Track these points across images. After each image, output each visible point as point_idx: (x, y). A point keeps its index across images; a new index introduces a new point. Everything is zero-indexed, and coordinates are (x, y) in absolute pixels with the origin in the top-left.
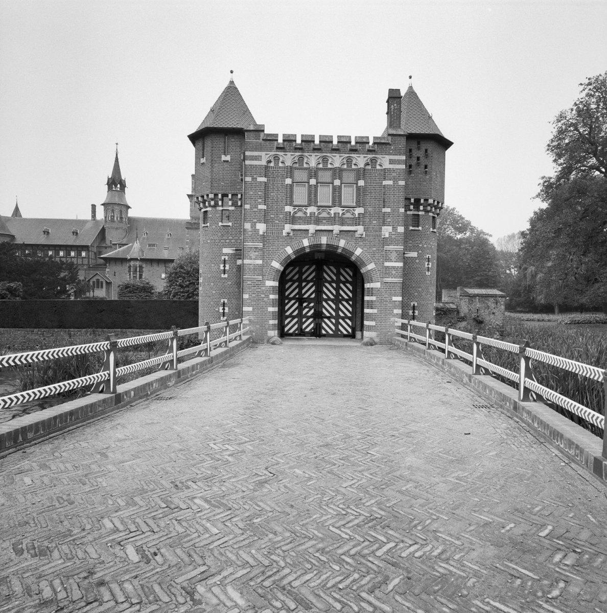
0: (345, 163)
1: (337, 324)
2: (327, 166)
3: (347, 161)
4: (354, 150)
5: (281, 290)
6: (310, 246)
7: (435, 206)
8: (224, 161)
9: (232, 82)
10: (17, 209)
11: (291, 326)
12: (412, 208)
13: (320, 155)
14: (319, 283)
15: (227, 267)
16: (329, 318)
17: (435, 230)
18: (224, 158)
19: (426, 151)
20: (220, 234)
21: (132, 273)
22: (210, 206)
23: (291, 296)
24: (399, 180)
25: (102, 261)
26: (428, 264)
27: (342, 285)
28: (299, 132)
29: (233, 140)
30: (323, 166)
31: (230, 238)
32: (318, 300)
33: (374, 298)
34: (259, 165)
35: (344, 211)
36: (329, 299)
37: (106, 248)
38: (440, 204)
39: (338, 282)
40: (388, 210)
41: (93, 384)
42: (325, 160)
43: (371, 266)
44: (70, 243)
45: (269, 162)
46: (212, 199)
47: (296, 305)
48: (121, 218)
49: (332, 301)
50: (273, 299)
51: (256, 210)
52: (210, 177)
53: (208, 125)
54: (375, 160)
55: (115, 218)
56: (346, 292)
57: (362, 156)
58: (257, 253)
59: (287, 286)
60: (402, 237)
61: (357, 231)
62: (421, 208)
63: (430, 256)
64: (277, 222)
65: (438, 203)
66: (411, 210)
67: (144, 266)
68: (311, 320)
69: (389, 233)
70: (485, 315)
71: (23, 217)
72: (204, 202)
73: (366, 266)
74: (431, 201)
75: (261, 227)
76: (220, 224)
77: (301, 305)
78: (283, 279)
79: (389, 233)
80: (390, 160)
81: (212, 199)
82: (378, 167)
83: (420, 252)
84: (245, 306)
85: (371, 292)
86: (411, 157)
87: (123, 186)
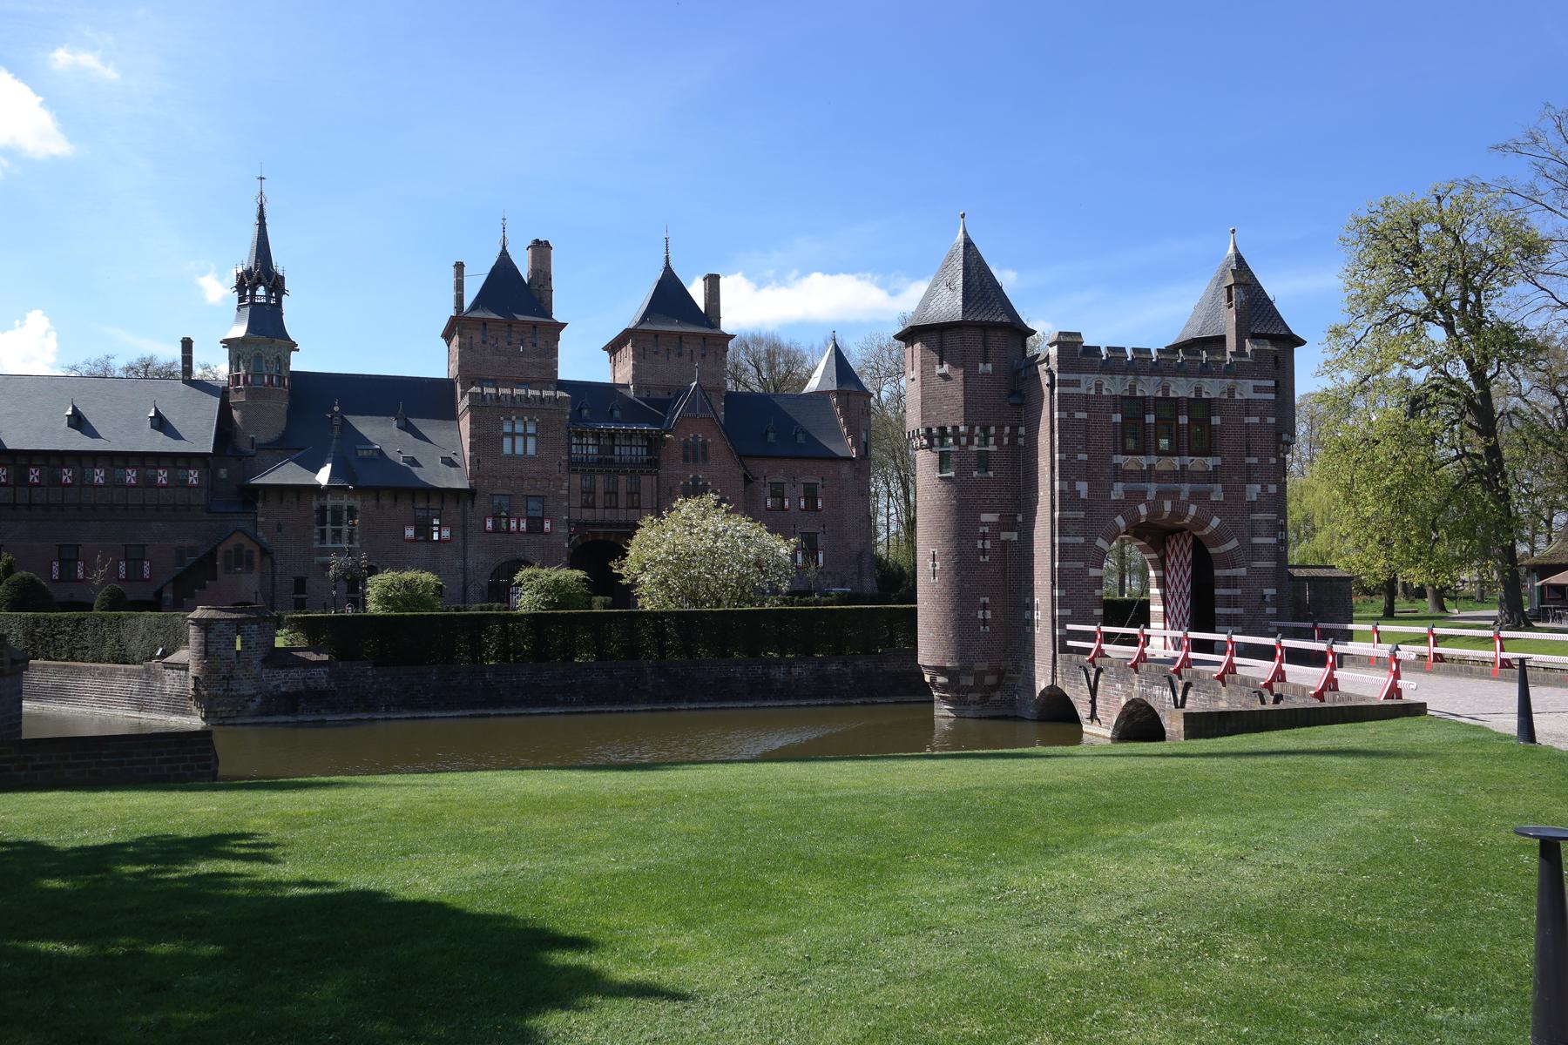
31: (992, 496)
51: (1074, 461)
58: (1077, 527)
62: (992, 440)
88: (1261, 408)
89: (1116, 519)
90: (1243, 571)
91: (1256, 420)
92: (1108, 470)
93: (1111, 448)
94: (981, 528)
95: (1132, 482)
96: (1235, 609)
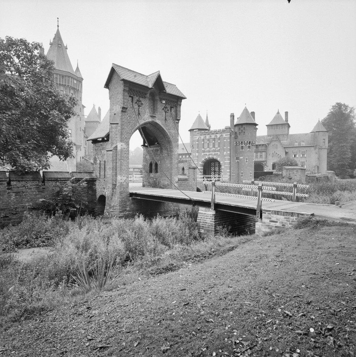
4: (217, 133)
9: (246, 107)
53: (237, 123)
70: (292, 176)
74: (246, 142)
75: (197, 154)
77: (215, 173)
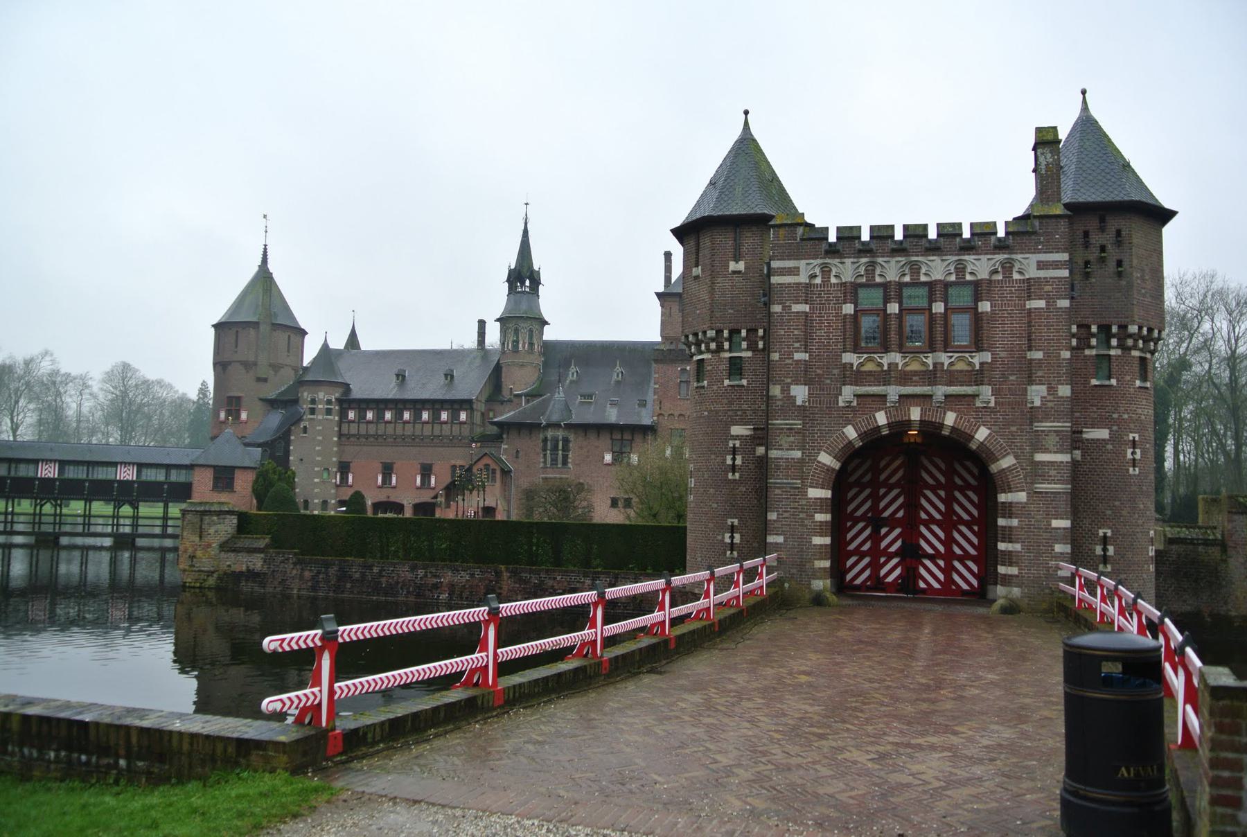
0: (952, 271)
1: (948, 570)
2: (919, 279)
3: (956, 268)
5: (837, 505)
6: (889, 425)
7: (1143, 338)
8: (734, 272)
10: (353, 334)
11: (858, 572)
12: (1095, 344)
13: (903, 259)
14: (912, 490)
15: (739, 461)
16: (932, 558)
17: (1148, 384)
18: (733, 266)
19: (1119, 233)
20: (725, 401)
21: (548, 452)
22: (708, 350)
23: (859, 513)
24: (1057, 299)
25: (495, 429)
26: (1133, 453)
27: (957, 494)
28: (865, 221)
29: (749, 234)
30: (911, 279)
31: (745, 407)
32: (910, 527)
33: (1015, 522)
34: (794, 284)
35: (953, 360)
36: (932, 520)
37: (502, 404)
38: (1156, 332)
39: (950, 487)
40: (1039, 355)
41: (466, 670)
42: (915, 269)
43: (1007, 462)
44: (439, 395)
45: (813, 276)
46: (713, 340)
47: (868, 532)
48: (531, 344)
49: (938, 525)
50: (820, 522)
51: (789, 361)
52: (708, 301)
53: (707, 212)
54: (1010, 263)
55: (520, 345)
56: (966, 507)
57: (984, 258)
58: (792, 439)
59: (850, 495)
60: (1067, 405)
61: (978, 396)
62: (1114, 342)
63: (1137, 436)
64: (828, 381)
65: (1150, 330)
66: (1093, 347)
67: (571, 437)
68: (895, 561)
69: (1042, 397)
71: (363, 348)
72: (698, 344)
73: (998, 460)
74: (1133, 329)
75: (800, 393)
76: (727, 382)
78: (840, 482)
79: (1042, 397)
80: (1038, 262)
81: (713, 340)
82: (1016, 276)
83: (1115, 428)
84: (770, 534)
85: (1009, 509)
86: (1087, 247)
87: (536, 281)
88: (1048, 288)
89: (845, 430)
90: (1022, 497)
91: (1041, 304)
92: (836, 372)
93: (840, 346)
94: (731, 442)
95: (869, 385)
96: (1010, 545)
